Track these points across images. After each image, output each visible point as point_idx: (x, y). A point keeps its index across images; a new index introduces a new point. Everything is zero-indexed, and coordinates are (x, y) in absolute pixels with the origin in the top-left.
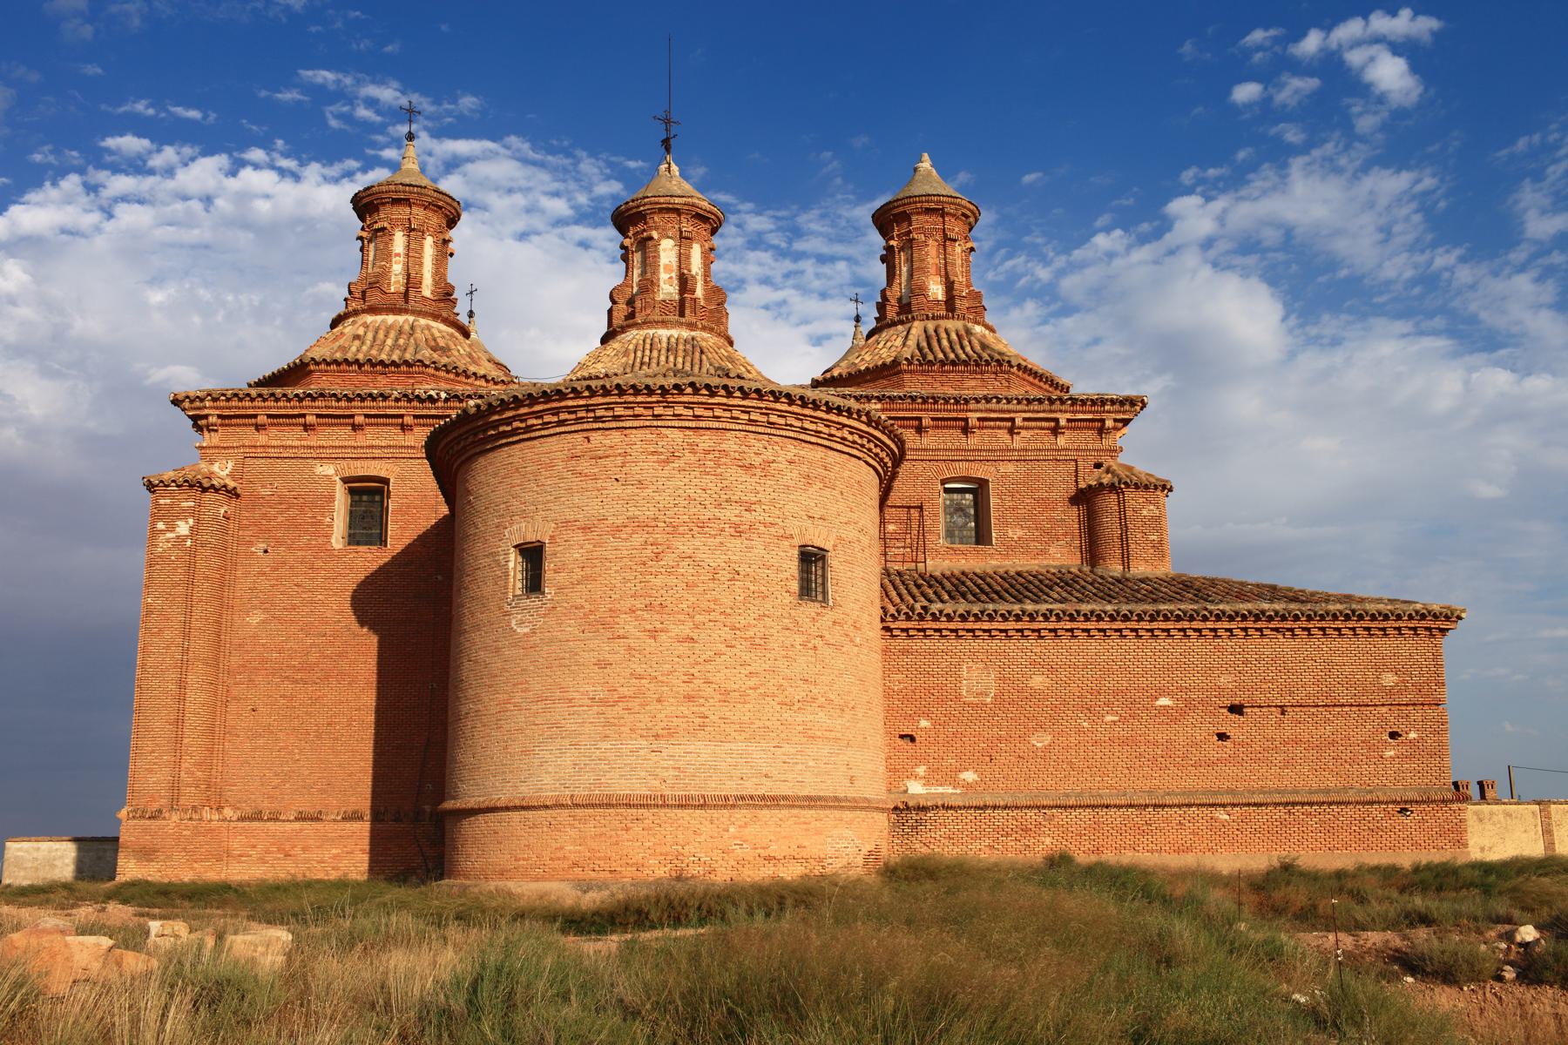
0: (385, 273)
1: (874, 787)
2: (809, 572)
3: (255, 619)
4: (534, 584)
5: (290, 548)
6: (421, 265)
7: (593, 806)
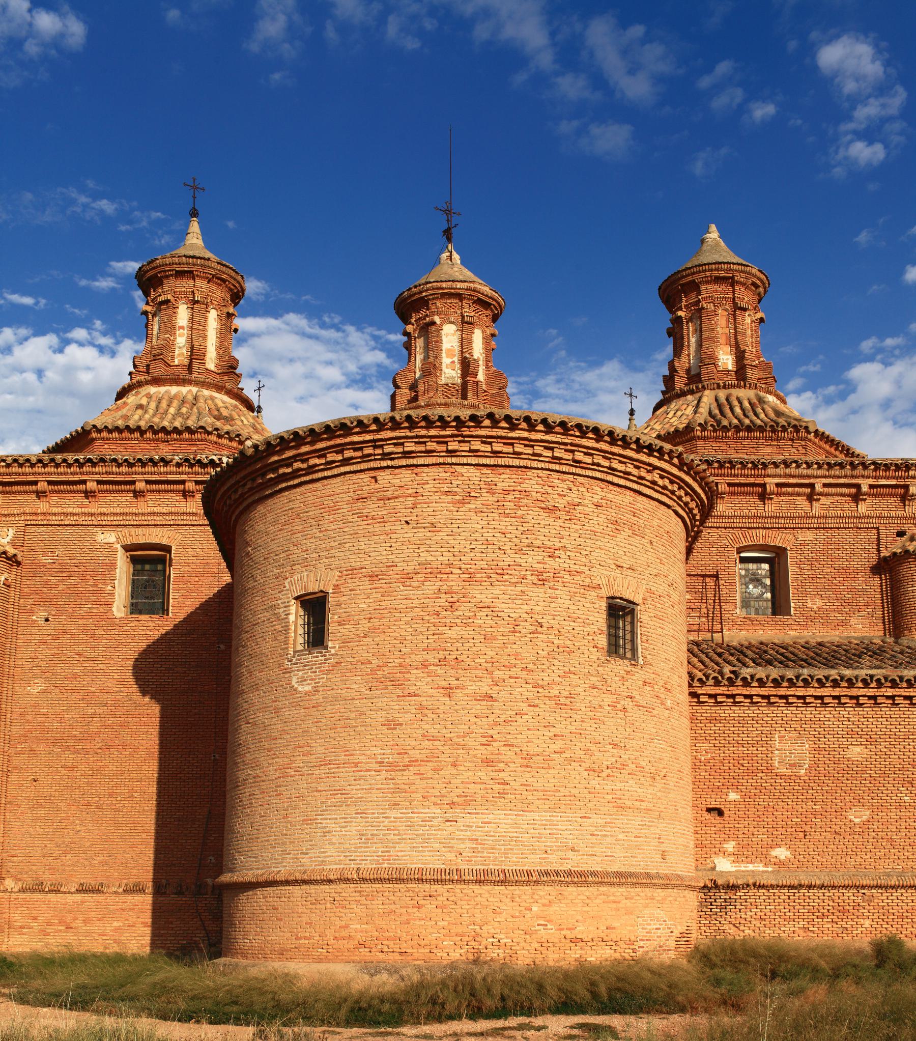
0: (168, 346)
1: (683, 864)
2: (617, 628)
3: (36, 688)
4: (317, 638)
5: (71, 616)
6: (205, 337)
7: (381, 880)
